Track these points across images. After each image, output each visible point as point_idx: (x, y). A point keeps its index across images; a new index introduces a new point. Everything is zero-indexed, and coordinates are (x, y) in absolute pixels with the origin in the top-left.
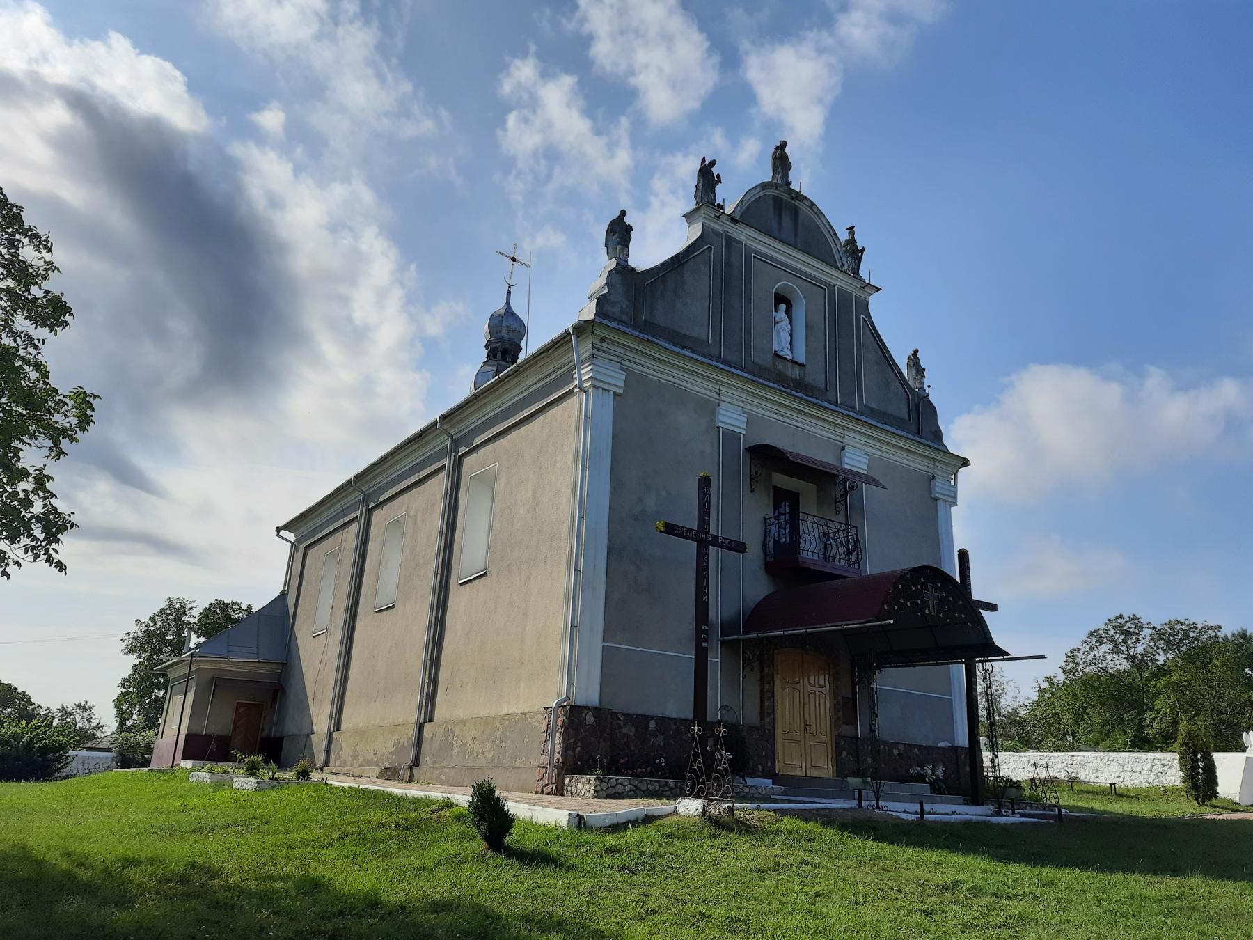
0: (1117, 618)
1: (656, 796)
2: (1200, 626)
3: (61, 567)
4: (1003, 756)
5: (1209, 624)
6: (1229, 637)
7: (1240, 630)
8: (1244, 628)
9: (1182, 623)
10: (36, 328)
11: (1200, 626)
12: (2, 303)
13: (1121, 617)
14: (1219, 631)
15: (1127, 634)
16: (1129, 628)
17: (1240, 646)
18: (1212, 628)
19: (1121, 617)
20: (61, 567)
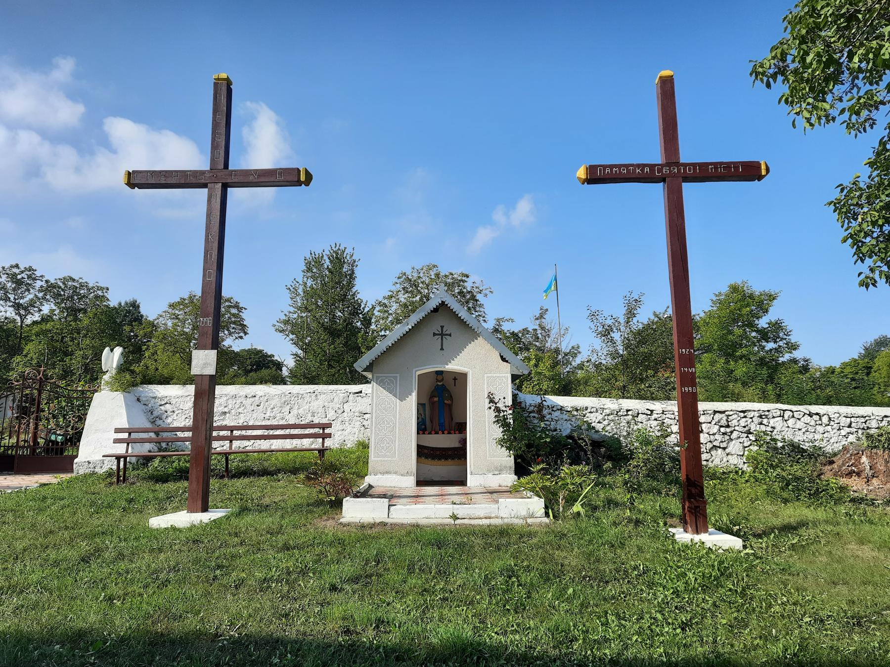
0: (12, 267)
1: (173, 642)
2: (91, 285)
3: (825, 205)
4: (115, 467)
5: (101, 285)
6: (123, 304)
7: (132, 300)
8: (135, 298)
9: (74, 280)
10: (656, 315)
11: (91, 285)
12: (1, 292)
13: (17, 266)
14: (106, 292)
15: (19, 283)
16: (23, 278)
17: (129, 312)
18: (102, 289)
19: (17, 266)
20: (825, 205)
